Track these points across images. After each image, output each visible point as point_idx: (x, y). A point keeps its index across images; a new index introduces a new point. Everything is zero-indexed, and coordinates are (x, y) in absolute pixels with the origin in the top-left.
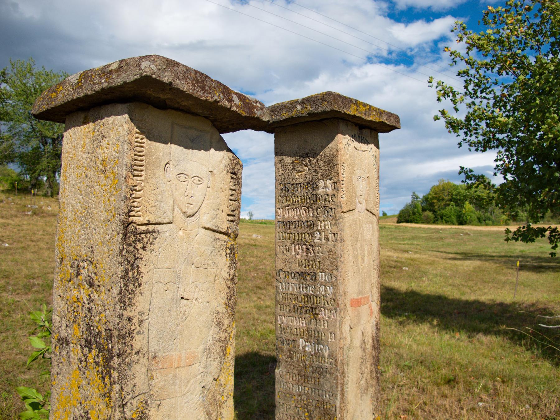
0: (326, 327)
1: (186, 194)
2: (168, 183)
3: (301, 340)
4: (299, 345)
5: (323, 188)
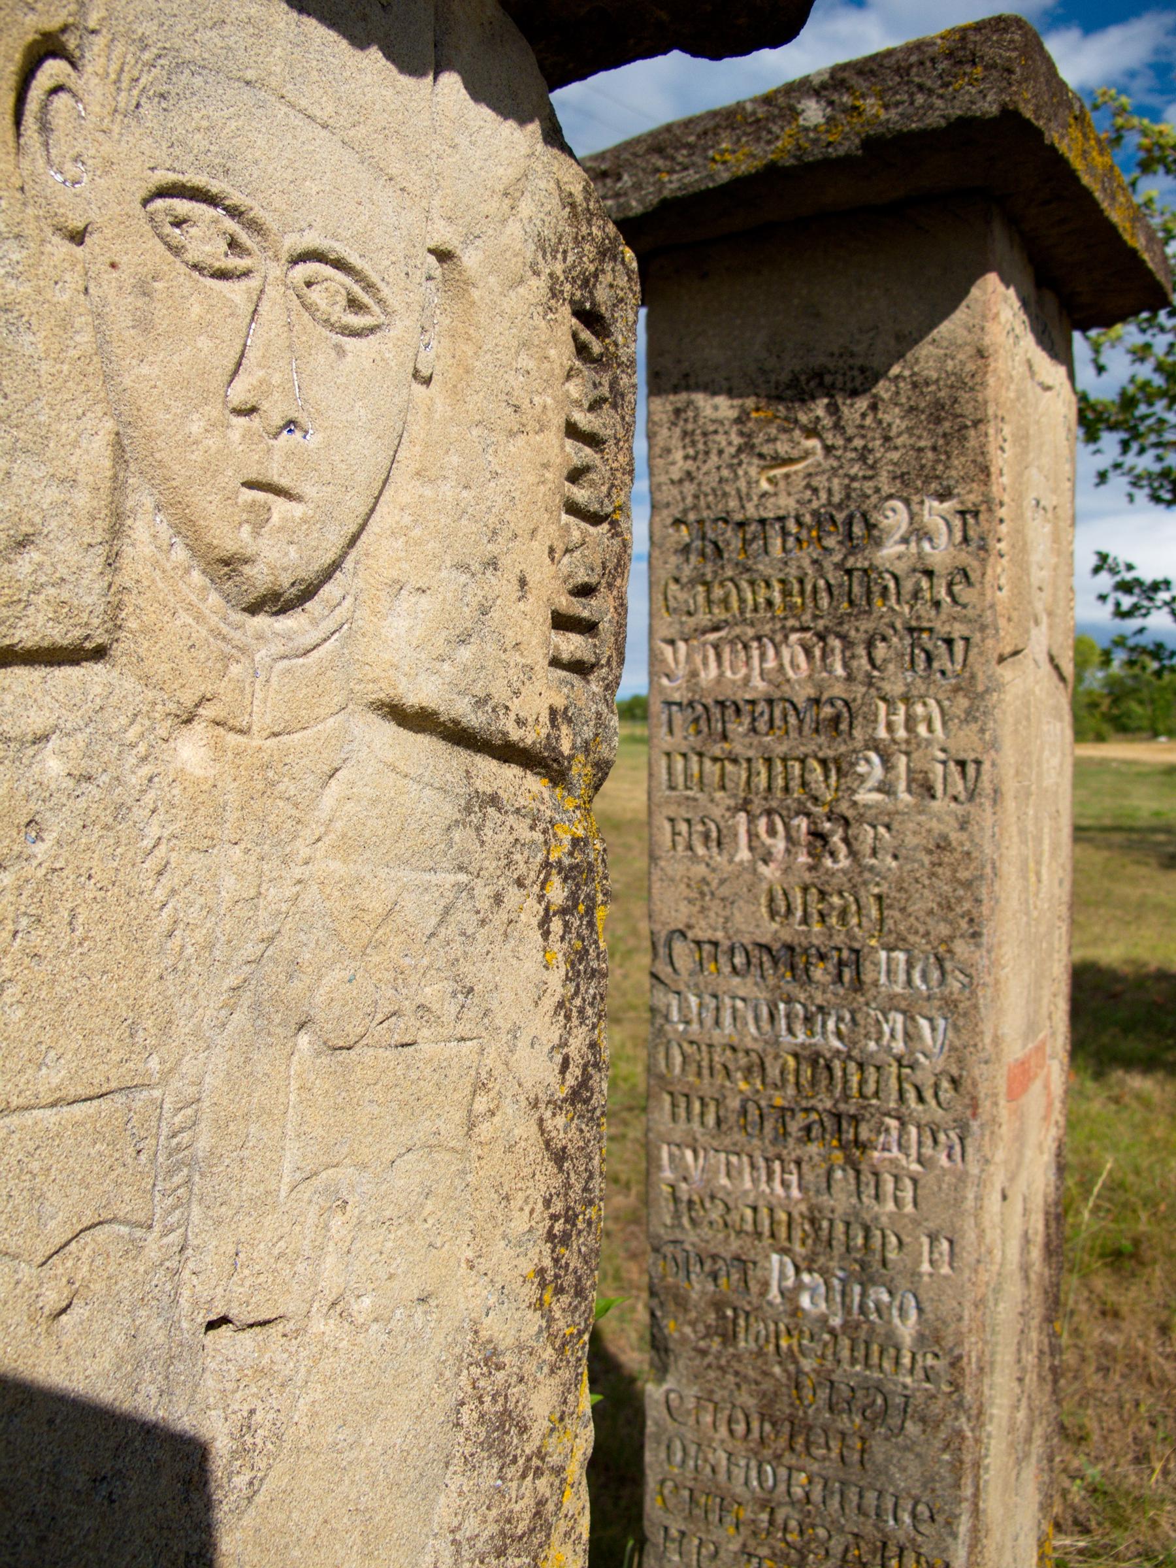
0: (909, 1208)
1: (239, 393)
2: (62, 248)
3: (775, 1257)
4: (766, 1285)
5: (905, 540)
